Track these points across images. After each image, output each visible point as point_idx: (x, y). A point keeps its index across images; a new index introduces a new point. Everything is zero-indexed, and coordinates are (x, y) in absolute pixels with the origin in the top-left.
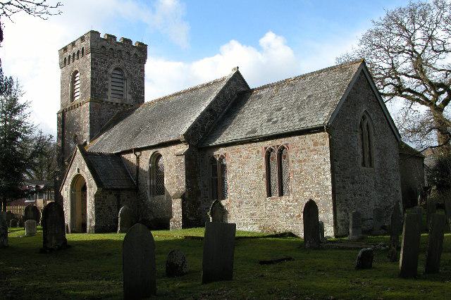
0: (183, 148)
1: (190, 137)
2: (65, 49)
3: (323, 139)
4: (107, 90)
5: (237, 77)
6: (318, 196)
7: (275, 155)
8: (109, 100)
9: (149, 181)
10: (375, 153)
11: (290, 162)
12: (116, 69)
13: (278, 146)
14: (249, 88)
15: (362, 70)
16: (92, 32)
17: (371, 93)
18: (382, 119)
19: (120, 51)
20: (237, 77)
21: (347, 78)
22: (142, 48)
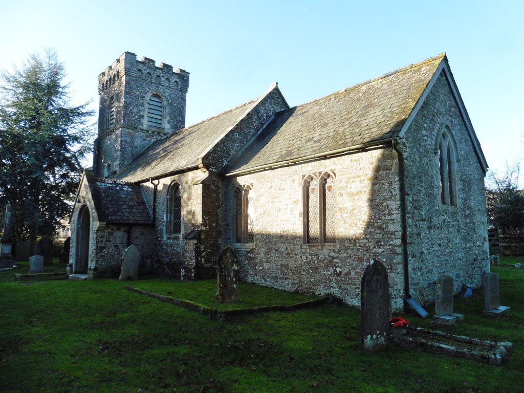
0: (202, 174)
1: (208, 161)
2: (103, 74)
3: (299, 230)
4: (143, 117)
5: (276, 95)
6: (379, 247)
7: (315, 185)
8: (145, 127)
9: (165, 215)
10: (458, 186)
11: (337, 195)
12: (155, 95)
13: (320, 173)
14: (288, 107)
15: (443, 70)
16: (127, 53)
17: (454, 103)
18: (466, 141)
19: (159, 76)
20: (276, 95)
21: (428, 73)
22: (184, 77)
